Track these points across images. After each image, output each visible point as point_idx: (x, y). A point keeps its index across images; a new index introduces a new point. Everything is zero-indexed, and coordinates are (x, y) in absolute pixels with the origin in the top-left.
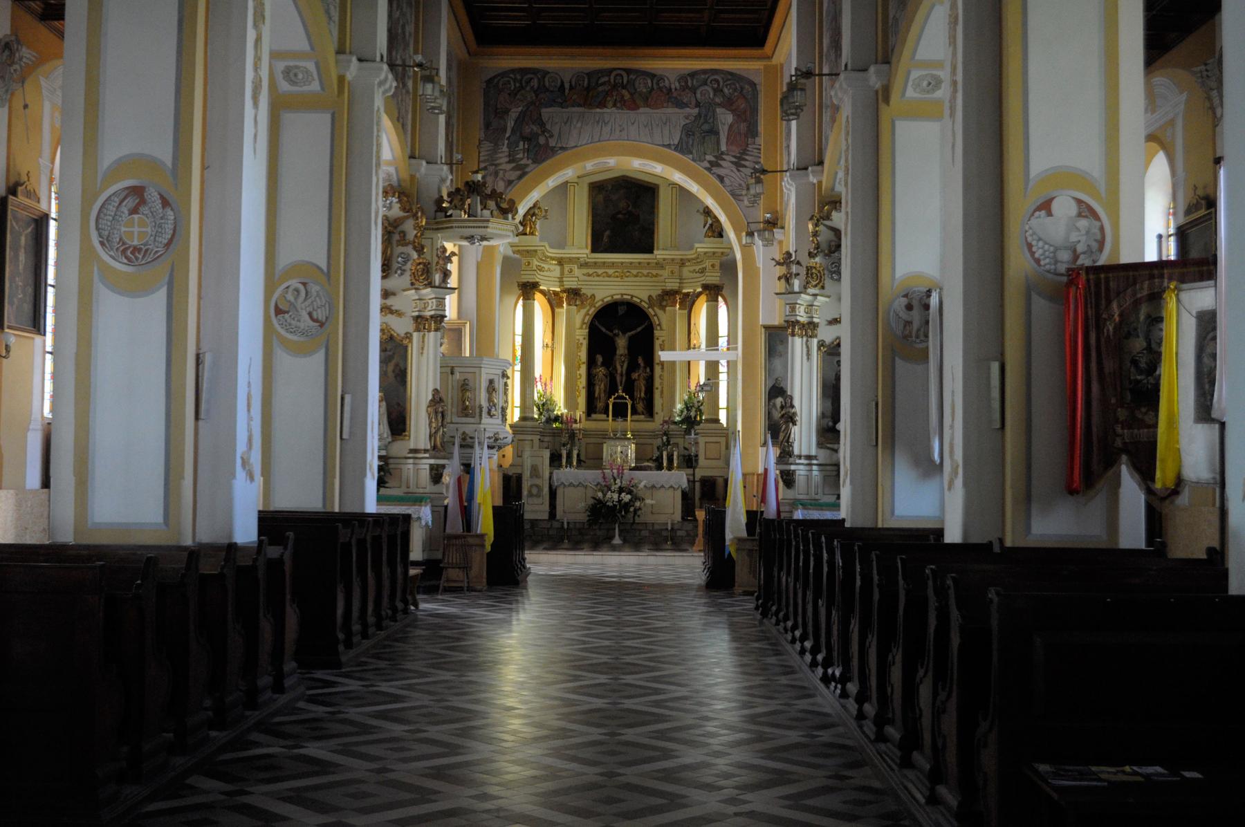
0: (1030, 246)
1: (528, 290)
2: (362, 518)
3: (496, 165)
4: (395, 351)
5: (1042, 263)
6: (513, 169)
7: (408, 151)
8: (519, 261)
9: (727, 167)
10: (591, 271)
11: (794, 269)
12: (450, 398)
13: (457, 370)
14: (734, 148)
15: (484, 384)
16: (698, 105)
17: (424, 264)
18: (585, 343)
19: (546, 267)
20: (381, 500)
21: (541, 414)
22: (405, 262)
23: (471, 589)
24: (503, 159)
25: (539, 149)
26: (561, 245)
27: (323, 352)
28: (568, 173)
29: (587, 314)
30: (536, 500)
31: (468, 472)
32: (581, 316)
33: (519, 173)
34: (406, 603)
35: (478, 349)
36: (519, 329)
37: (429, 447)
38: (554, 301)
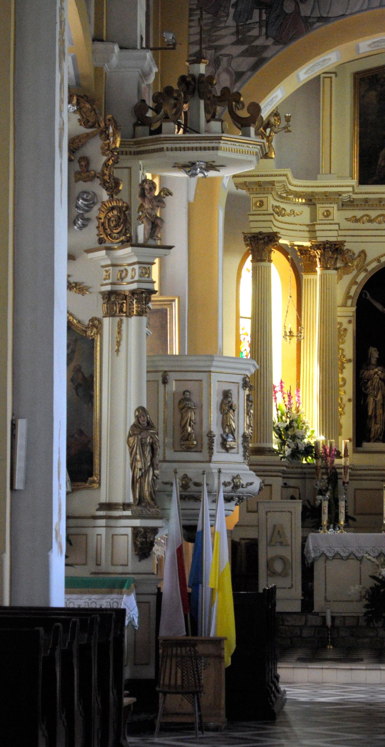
1: (260, 245)
2: (46, 616)
4: (82, 344)
6: (244, 54)
7: (92, 30)
8: (246, 199)
10: (359, 214)
12: (162, 418)
13: (172, 377)
15: (215, 399)
17: (120, 209)
18: (351, 329)
19: (288, 208)
20: (71, 584)
21: (283, 443)
22: (89, 208)
23: (204, 728)
26: (312, 172)
28: (331, 58)
29: (353, 282)
31: (190, 539)
32: (344, 286)
33: (252, 60)
35: (190, 341)
36: (246, 308)
37: (131, 499)
38: (300, 262)
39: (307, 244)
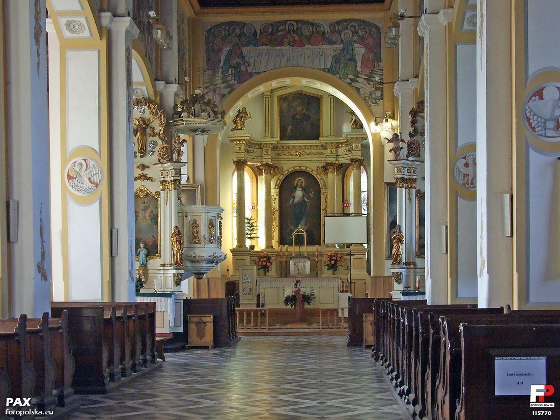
0: (528, 119)
3: (215, 85)
5: (536, 130)
6: (226, 87)
9: (361, 82)
11: (401, 144)
14: (366, 69)
16: (342, 42)
19: (251, 150)
22: (154, 148)
24: (218, 80)
25: (242, 76)
27: (98, 202)
29: (279, 179)
30: (248, 296)
33: (229, 90)
34: (153, 356)
38: (257, 171)
39: (259, 164)
